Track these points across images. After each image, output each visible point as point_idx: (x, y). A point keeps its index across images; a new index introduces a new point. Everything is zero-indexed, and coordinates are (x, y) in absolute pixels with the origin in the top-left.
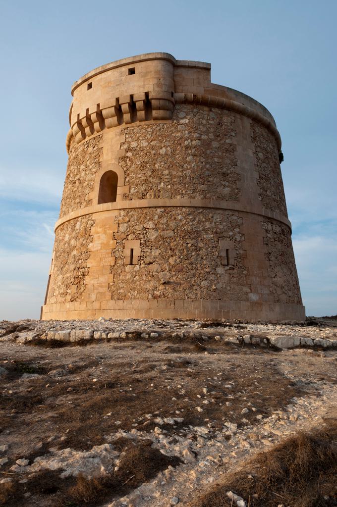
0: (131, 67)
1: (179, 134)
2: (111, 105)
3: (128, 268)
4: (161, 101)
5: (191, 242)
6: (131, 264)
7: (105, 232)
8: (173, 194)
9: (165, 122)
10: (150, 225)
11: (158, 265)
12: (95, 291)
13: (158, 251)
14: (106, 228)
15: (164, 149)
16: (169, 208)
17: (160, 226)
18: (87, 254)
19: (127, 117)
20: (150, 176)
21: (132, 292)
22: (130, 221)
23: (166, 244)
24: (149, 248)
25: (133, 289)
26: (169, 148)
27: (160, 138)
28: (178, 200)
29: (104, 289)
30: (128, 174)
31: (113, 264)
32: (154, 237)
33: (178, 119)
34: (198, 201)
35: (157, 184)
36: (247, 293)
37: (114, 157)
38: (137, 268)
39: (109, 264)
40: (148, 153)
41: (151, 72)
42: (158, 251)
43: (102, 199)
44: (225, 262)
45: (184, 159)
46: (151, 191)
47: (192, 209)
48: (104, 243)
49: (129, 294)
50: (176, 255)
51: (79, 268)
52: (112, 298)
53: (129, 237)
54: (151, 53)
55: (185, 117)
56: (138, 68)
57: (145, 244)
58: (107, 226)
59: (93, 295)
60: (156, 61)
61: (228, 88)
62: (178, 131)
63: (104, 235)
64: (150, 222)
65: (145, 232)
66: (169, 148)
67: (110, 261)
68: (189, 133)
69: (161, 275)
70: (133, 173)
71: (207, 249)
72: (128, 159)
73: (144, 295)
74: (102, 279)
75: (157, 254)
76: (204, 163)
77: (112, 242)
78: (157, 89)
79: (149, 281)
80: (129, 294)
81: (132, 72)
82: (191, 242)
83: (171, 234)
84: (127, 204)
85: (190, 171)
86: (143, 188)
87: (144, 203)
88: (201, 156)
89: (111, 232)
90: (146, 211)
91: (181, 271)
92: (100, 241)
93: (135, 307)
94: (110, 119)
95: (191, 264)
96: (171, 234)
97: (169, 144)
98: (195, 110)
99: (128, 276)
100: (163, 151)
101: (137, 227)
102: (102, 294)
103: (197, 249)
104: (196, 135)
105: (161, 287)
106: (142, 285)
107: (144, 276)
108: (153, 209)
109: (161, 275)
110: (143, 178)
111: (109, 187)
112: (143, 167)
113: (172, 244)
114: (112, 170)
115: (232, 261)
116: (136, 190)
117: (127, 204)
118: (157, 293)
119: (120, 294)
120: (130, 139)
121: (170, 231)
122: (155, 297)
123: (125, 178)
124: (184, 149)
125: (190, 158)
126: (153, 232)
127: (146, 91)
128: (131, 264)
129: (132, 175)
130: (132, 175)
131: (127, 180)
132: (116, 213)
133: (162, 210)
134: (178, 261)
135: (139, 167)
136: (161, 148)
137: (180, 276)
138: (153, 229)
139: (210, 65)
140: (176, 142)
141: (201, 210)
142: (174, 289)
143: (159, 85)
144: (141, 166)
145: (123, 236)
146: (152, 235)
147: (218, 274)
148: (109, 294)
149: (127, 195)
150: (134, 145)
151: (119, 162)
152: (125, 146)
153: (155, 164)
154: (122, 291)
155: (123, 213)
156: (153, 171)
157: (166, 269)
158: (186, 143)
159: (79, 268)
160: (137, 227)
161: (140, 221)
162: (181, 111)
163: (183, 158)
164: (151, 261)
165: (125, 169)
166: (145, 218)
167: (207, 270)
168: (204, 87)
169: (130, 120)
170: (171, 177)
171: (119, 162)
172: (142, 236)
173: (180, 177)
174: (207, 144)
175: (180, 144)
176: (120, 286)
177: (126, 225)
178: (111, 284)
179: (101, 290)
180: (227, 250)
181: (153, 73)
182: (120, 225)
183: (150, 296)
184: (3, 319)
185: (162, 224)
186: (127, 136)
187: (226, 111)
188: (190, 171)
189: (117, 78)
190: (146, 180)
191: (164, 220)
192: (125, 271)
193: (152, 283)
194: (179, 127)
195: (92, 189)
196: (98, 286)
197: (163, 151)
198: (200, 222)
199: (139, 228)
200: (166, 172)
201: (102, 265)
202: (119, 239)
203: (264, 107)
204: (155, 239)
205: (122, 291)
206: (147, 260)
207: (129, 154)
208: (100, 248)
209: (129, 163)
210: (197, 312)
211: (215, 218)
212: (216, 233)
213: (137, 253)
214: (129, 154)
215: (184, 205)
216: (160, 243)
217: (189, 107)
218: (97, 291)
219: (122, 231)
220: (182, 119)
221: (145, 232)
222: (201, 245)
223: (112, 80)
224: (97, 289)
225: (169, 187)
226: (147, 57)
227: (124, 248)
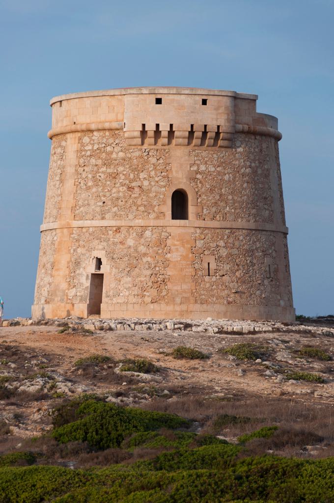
0: (205, 97)
1: (237, 162)
2: (185, 129)
3: (207, 278)
4: (229, 134)
5: (249, 259)
6: (209, 275)
7: (183, 246)
8: (237, 217)
9: (227, 150)
10: (222, 243)
11: (229, 277)
12: (179, 295)
13: (229, 266)
14: (184, 242)
15: (227, 175)
16: (234, 230)
17: (229, 245)
18: (166, 263)
19: (195, 141)
20: (219, 200)
21: (212, 298)
22: (204, 239)
23: (234, 260)
24: (222, 263)
25: (213, 296)
26: (231, 175)
27: (224, 165)
28: (240, 223)
29: (188, 294)
30: (200, 196)
31: (194, 274)
32: (226, 253)
33: (236, 147)
34: (252, 225)
35: (225, 208)
36: (279, 301)
37: (184, 176)
38: (214, 279)
39: (190, 274)
40: (215, 178)
41: (222, 107)
42: (229, 266)
43: (174, 217)
44: (268, 276)
45: (242, 185)
46: (220, 213)
47: (249, 231)
48: (183, 255)
49: (210, 300)
50: (240, 270)
51: (156, 274)
52: (196, 302)
53: (206, 252)
54: (223, 91)
55: (240, 146)
56: (211, 100)
57: (219, 259)
58: (185, 241)
59: (177, 299)
60: (226, 97)
61: (265, 115)
62: (236, 160)
63: (182, 248)
64: (221, 241)
65: (218, 249)
66: (231, 175)
67: (190, 271)
68: (244, 162)
69: (231, 285)
70: (204, 195)
71: (258, 265)
72: (199, 181)
73: (221, 301)
74: (185, 287)
75: (228, 268)
76: (254, 190)
77: (191, 255)
78: (227, 124)
79: (224, 290)
80: (210, 300)
81: (204, 102)
82: (249, 259)
83: (236, 252)
84: (201, 223)
85: (246, 197)
86: (214, 209)
87: (215, 224)
88: (252, 183)
89: (189, 246)
90: (218, 231)
91: (244, 282)
92: (177, 255)
93: (217, 310)
94: (181, 139)
95: (250, 277)
96: (236, 252)
97: (231, 171)
98: (247, 139)
99: (208, 285)
100: (226, 177)
101: (211, 244)
102: (187, 299)
103: (253, 265)
104: (248, 164)
105: (232, 295)
106: (219, 293)
107: (220, 286)
108: (223, 230)
109: (231, 285)
110: (213, 201)
111: (179, 204)
112: (211, 190)
113: (237, 261)
114: (183, 188)
115: (272, 275)
116: (208, 212)
117: (201, 223)
118: (230, 300)
119: (202, 299)
120: (198, 162)
121: (235, 249)
122: (229, 303)
123: (198, 199)
124: (241, 176)
125: (245, 185)
126: (224, 250)
127: (219, 125)
128: (209, 275)
129: (204, 197)
130: (204, 197)
131: (199, 200)
132: (192, 230)
133: (230, 231)
134: (242, 274)
135: (209, 190)
136: (225, 174)
137: (244, 287)
138: (224, 247)
139: (257, 96)
140: (236, 169)
141: (254, 232)
142: (241, 297)
143: (228, 120)
144: (211, 189)
145: (200, 251)
146: (224, 252)
147: (265, 285)
148: (192, 300)
149: (200, 214)
150: (203, 168)
151: (191, 183)
152: (195, 168)
153: (221, 189)
154: (203, 297)
155: (198, 231)
156: (221, 195)
157: (234, 281)
158: (242, 171)
159: (156, 274)
160: (211, 244)
161: (214, 239)
162: (238, 140)
163: (241, 185)
164: (224, 274)
165: (197, 190)
166: (218, 237)
167: (259, 282)
168: (252, 117)
169: (187, 144)
170: (234, 202)
171: (191, 183)
172: (216, 253)
173: (239, 202)
174: (255, 172)
175: (239, 172)
176: (202, 293)
177: (202, 241)
178: (194, 291)
179: (185, 295)
180: (269, 265)
181: (223, 108)
182: (197, 241)
183: (225, 302)
184: (296, 308)
185: (230, 243)
186: (196, 159)
187: (264, 138)
188: (246, 197)
189: (191, 105)
190: (216, 203)
191: (231, 240)
192: (204, 281)
193: (226, 292)
194: (237, 155)
195: (164, 202)
196: (182, 291)
197: (226, 177)
198: (254, 242)
199: (213, 245)
200: (230, 197)
201: (184, 274)
202: (197, 254)
203: (271, 116)
204: (226, 255)
205: (203, 297)
206: (221, 273)
207: (199, 176)
208: (179, 259)
209: (200, 185)
210: (256, 315)
211: (262, 238)
212: (263, 251)
213: (213, 266)
214: (199, 176)
215: (239, 228)
216: (230, 259)
217: (243, 136)
218: (182, 296)
219: (200, 246)
220: (238, 147)
221: (218, 249)
222: (255, 261)
223: (186, 104)
224: (181, 294)
225: (233, 210)
226: (220, 94)
227: (202, 261)
